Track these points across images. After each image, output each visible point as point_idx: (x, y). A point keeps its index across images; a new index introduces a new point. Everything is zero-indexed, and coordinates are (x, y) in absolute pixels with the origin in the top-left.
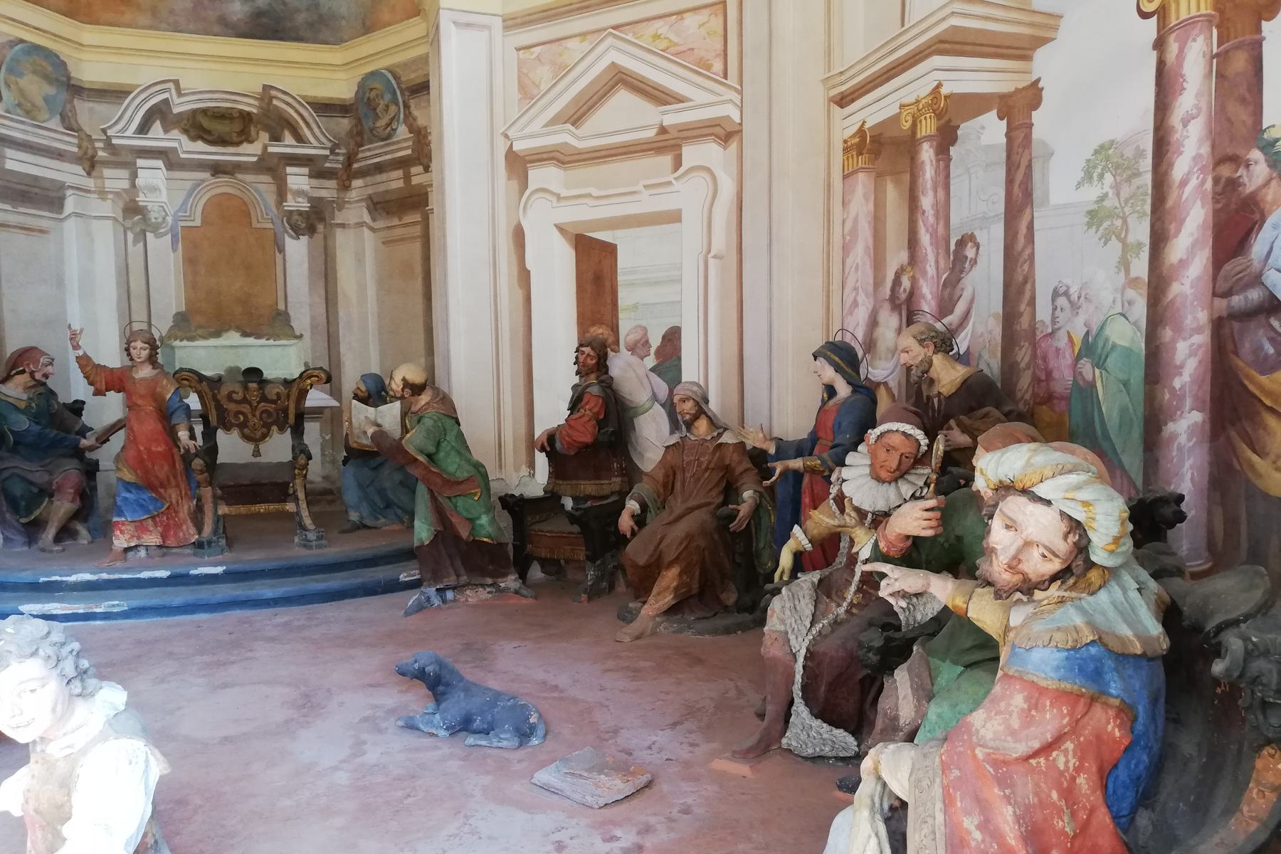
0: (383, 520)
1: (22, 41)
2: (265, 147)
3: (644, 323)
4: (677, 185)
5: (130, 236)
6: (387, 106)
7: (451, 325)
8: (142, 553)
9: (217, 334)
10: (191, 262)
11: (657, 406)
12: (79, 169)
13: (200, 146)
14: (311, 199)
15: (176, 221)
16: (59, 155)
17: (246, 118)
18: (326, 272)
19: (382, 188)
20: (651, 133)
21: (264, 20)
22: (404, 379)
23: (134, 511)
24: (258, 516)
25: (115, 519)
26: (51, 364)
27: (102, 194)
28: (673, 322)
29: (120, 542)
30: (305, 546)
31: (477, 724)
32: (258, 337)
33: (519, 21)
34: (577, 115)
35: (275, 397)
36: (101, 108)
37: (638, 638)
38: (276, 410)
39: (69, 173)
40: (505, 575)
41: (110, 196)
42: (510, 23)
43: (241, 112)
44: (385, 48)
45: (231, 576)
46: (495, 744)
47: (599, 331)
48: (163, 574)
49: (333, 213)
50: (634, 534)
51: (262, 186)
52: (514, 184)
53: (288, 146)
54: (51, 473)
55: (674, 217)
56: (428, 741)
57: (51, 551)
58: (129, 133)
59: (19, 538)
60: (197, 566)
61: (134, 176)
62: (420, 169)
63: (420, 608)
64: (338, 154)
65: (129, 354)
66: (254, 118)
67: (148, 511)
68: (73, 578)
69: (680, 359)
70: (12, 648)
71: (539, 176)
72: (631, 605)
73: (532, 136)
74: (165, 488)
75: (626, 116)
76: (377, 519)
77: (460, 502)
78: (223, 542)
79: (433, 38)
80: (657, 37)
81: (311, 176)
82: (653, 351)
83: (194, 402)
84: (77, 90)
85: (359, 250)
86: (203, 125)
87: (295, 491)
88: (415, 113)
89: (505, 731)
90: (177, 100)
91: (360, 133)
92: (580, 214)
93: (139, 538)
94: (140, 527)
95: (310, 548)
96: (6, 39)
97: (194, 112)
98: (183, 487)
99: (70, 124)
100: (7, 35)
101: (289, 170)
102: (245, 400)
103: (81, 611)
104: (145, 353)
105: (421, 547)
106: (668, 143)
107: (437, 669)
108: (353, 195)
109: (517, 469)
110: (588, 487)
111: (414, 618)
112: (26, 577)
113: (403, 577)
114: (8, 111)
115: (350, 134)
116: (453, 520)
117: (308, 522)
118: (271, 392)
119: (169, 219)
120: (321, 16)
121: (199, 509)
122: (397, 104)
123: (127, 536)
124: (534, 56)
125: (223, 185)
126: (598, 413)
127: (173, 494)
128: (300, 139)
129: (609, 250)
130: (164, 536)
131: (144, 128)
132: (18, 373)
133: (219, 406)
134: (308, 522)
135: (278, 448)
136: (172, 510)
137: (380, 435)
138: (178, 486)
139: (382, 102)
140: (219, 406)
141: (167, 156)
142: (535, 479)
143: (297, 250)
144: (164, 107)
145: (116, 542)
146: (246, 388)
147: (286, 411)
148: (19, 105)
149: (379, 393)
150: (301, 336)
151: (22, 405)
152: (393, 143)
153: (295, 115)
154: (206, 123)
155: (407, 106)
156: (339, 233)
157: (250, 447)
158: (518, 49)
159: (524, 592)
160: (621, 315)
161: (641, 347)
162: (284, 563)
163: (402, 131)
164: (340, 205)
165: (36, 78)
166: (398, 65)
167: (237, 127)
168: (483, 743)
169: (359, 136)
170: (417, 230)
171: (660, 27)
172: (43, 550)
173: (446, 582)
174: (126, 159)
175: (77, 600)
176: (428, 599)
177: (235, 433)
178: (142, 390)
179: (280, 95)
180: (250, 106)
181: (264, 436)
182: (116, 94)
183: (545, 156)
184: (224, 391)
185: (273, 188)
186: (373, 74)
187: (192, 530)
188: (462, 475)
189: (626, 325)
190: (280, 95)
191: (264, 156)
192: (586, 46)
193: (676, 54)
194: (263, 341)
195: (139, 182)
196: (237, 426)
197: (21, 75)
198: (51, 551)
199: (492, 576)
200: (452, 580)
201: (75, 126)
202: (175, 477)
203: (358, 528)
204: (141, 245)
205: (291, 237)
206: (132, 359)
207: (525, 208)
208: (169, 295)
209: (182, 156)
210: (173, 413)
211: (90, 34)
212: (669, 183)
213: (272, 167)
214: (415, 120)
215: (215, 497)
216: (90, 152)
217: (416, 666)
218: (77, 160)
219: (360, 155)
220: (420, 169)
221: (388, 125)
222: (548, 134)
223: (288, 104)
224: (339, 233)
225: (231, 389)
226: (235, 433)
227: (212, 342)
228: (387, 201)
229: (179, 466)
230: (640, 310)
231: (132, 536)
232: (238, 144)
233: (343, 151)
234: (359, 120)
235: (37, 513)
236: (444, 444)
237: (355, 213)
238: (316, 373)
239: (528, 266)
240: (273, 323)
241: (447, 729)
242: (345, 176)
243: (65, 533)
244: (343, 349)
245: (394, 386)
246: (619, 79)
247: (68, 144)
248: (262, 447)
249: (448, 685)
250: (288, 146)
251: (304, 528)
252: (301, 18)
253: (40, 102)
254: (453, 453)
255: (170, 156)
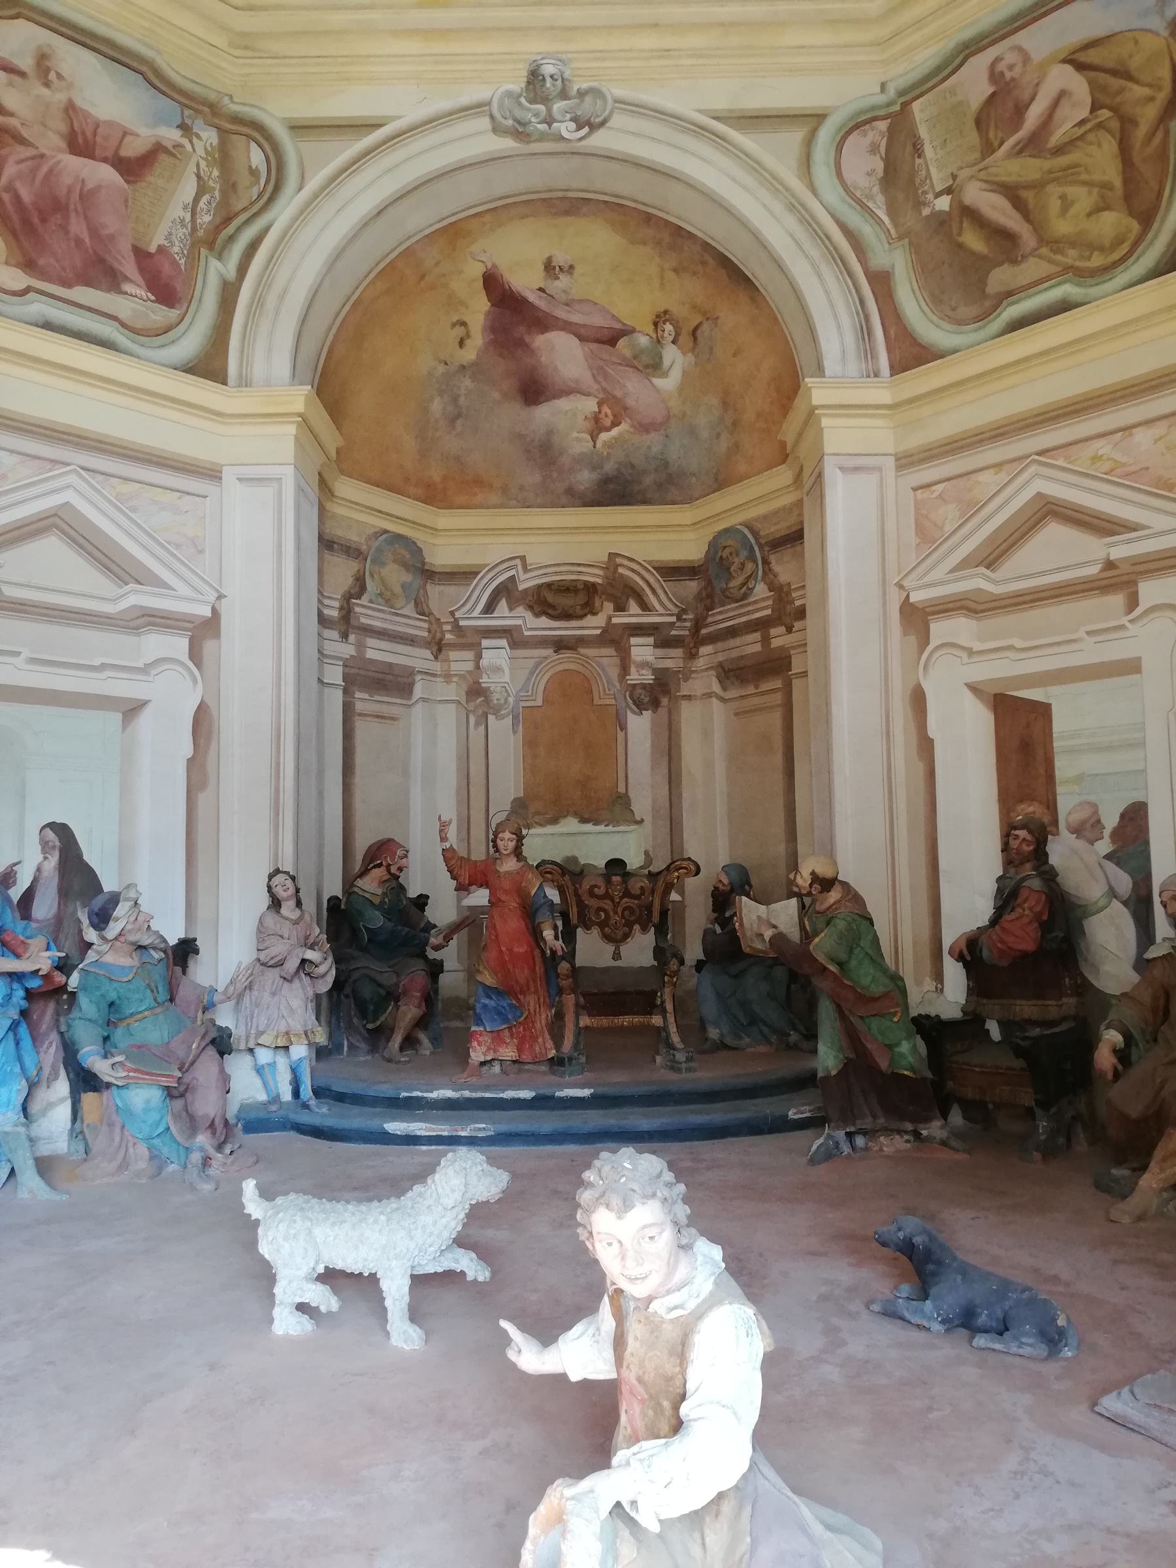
0: (747, 1040)
1: (386, 531)
2: (610, 618)
3: (1092, 798)
4: (1133, 629)
5: (472, 719)
6: (743, 564)
7: (838, 807)
8: (497, 1068)
9: (554, 821)
10: (530, 744)
11: (1116, 905)
12: (427, 654)
13: (544, 621)
14: (655, 671)
15: (517, 701)
16: (411, 641)
17: (591, 589)
18: (669, 751)
19: (735, 654)
20: (1094, 570)
21: (611, 486)
22: (813, 873)
23: (493, 1020)
24: (621, 1029)
25: (473, 1028)
26: (406, 856)
27: (448, 677)
28: (1138, 796)
29: (477, 1054)
30: (672, 1068)
31: (983, 1319)
32: (597, 823)
33: (915, 458)
34: (993, 555)
35: (638, 892)
36: (450, 590)
37: (1140, 1218)
38: (640, 907)
39: (418, 658)
40: (927, 1120)
41: (455, 679)
42: (904, 461)
43: (586, 583)
44: (754, 499)
45: (599, 1101)
46: (1014, 1350)
47: (1028, 810)
48: (526, 1094)
49: (679, 684)
50: (1117, 1075)
51: (606, 658)
52: (912, 640)
53: (633, 615)
54: (398, 975)
55: (1132, 667)
56: (916, 1335)
57: (398, 1062)
58: (476, 614)
59: (363, 1046)
60: (562, 1087)
61: (479, 656)
62: (782, 629)
63: (829, 1155)
64: (685, 620)
65: (495, 846)
66: (599, 588)
67: (505, 1020)
68: (434, 1095)
69: (1147, 843)
70: (636, 1187)
71: (940, 629)
72: (1114, 1171)
73: (933, 585)
74: (525, 997)
75: (1058, 553)
76: (740, 1038)
77: (875, 1024)
78: (583, 1059)
79: (811, 484)
80: (1096, 459)
81: (656, 646)
82: (1107, 833)
83: (553, 895)
84: (429, 574)
85: (708, 723)
86: (562, 598)
87: (663, 1002)
88: (776, 568)
89: (1027, 1334)
90: (522, 576)
91: (710, 596)
92: (996, 670)
93: (495, 1051)
94: (497, 1037)
95: (679, 1071)
96: (373, 530)
97: (539, 587)
98: (541, 993)
99: (422, 610)
100: (374, 526)
101: (633, 640)
102: (606, 896)
103: (445, 1134)
104: (512, 845)
105: (827, 1078)
106: (1120, 581)
107: (927, 1239)
108: (700, 663)
109: (919, 983)
110: (1026, 1008)
111: (823, 1168)
112: (386, 1090)
113: (792, 1114)
114: (371, 601)
115: (699, 598)
116: (869, 1046)
117: (675, 1039)
118: (636, 885)
119: (511, 700)
120: (670, 475)
121: (559, 1016)
122: (755, 561)
123: (484, 1048)
124: (936, 494)
125: (567, 661)
126: (1041, 913)
127: (531, 1001)
128: (645, 606)
129: (1043, 711)
130: (520, 1050)
131: (489, 608)
132: (375, 867)
133: (581, 904)
134: (675, 1039)
135: (639, 950)
136: (529, 1022)
137: (779, 939)
138: (536, 992)
139: (736, 560)
140: (581, 904)
141: (512, 636)
142: (951, 994)
143: (640, 727)
144: (510, 585)
145: (472, 1054)
146: (608, 882)
147: (649, 908)
148: (381, 595)
149: (742, 886)
150: (642, 821)
151: (377, 901)
152: (749, 604)
153: (641, 582)
154: (550, 598)
155: (766, 562)
156: (684, 704)
157: (610, 948)
158: (915, 489)
159: (953, 1143)
160: (1060, 789)
161: (1088, 828)
162: (653, 1088)
163: (761, 590)
164: (687, 675)
165: (396, 567)
166: (756, 519)
167: (581, 599)
168: (997, 1346)
169: (708, 600)
170: (778, 698)
171: (1103, 447)
172: (389, 1060)
173: (860, 1124)
174: (471, 640)
175: (446, 1120)
176: (837, 1144)
177: (595, 932)
178: (506, 885)
179: (626, 562)
180: (595, 577)
181: (626, 936)
182: (463, 575)
183: (951, 606)
184: (586, 885)
185: (617, 661)
186: (726, 531)
187: (550, 1044)
188: (877, 990)
189: (1067, 802)
190: (626, 562)
191: (608, 629)
192: (1003, 477)
193: (1126, 475)
194: (601, 828)
195: (484, 662)
196: (599, 924)
197: (383, 564)
198: (398, 1062)
199: (912, 1121)
200: (867, 1123)
201: (426, 611)
202: (535, 981)
203: (718, 1049)
204: (483, 727)
205: (634, 712)
206: (497, 851)
207: (926, 667)
208: (508, 783)
209: (526, 633)
210: (537, 910)
211: (445, 519)
212: (1122, 627)
213: (616, 639)
214: (776, 576)
215: (577, 1005)
216: (438, 635)
217: (901, 1235)
218: (427, 644)
219: (710, 620)
220: (782, 629)
221: (744, 584)
222: (956, 580)
223: (633, 571)
224: (684, 704)
225: (593, 883)
226: (595, 932)
227: (549, 829)
228: (741, 669)
229: (539, 968)
230: (1085, 780)
231: (489, 1049)
232: (582, 617)
233: (691, 616)
234: (709, 583)
235: (382, 1019)
236: (856, 951)
237: (703, 680)
238: (685, 864)
239: (931, 734)
240: (610, 807)
241: (943, 1322)
242: (692, 643)
243: (410, 1042)
244: (686, 835)
245: (799, 881)
246: (1050, 510)
247: (420, 629)
248: (624, 949)
249: (939, 1263)
250: (633, 615)
251: (671, 1046)
252: (648, 480)
253: (398, 590)
254: (866, 962)
255: (514, 634)
